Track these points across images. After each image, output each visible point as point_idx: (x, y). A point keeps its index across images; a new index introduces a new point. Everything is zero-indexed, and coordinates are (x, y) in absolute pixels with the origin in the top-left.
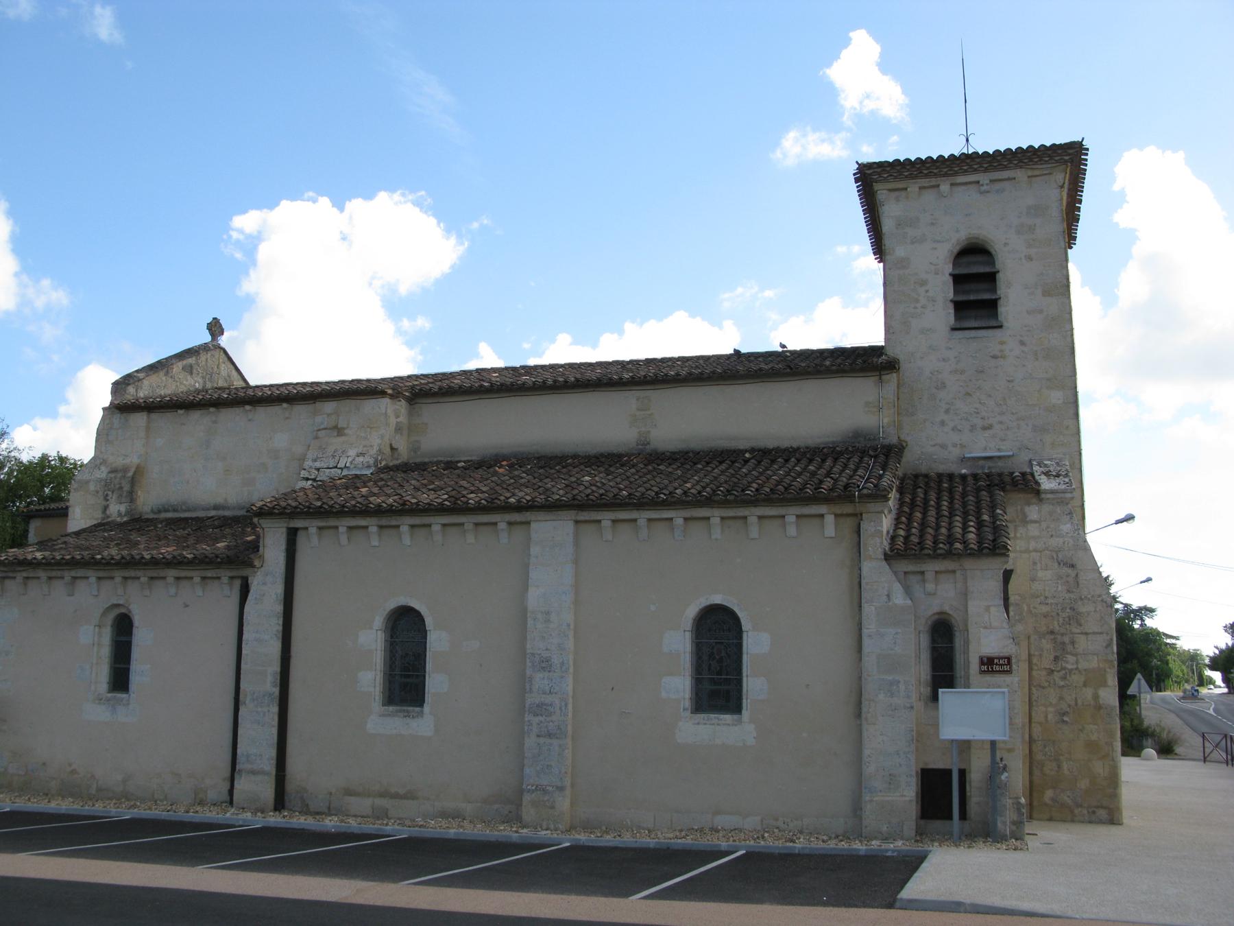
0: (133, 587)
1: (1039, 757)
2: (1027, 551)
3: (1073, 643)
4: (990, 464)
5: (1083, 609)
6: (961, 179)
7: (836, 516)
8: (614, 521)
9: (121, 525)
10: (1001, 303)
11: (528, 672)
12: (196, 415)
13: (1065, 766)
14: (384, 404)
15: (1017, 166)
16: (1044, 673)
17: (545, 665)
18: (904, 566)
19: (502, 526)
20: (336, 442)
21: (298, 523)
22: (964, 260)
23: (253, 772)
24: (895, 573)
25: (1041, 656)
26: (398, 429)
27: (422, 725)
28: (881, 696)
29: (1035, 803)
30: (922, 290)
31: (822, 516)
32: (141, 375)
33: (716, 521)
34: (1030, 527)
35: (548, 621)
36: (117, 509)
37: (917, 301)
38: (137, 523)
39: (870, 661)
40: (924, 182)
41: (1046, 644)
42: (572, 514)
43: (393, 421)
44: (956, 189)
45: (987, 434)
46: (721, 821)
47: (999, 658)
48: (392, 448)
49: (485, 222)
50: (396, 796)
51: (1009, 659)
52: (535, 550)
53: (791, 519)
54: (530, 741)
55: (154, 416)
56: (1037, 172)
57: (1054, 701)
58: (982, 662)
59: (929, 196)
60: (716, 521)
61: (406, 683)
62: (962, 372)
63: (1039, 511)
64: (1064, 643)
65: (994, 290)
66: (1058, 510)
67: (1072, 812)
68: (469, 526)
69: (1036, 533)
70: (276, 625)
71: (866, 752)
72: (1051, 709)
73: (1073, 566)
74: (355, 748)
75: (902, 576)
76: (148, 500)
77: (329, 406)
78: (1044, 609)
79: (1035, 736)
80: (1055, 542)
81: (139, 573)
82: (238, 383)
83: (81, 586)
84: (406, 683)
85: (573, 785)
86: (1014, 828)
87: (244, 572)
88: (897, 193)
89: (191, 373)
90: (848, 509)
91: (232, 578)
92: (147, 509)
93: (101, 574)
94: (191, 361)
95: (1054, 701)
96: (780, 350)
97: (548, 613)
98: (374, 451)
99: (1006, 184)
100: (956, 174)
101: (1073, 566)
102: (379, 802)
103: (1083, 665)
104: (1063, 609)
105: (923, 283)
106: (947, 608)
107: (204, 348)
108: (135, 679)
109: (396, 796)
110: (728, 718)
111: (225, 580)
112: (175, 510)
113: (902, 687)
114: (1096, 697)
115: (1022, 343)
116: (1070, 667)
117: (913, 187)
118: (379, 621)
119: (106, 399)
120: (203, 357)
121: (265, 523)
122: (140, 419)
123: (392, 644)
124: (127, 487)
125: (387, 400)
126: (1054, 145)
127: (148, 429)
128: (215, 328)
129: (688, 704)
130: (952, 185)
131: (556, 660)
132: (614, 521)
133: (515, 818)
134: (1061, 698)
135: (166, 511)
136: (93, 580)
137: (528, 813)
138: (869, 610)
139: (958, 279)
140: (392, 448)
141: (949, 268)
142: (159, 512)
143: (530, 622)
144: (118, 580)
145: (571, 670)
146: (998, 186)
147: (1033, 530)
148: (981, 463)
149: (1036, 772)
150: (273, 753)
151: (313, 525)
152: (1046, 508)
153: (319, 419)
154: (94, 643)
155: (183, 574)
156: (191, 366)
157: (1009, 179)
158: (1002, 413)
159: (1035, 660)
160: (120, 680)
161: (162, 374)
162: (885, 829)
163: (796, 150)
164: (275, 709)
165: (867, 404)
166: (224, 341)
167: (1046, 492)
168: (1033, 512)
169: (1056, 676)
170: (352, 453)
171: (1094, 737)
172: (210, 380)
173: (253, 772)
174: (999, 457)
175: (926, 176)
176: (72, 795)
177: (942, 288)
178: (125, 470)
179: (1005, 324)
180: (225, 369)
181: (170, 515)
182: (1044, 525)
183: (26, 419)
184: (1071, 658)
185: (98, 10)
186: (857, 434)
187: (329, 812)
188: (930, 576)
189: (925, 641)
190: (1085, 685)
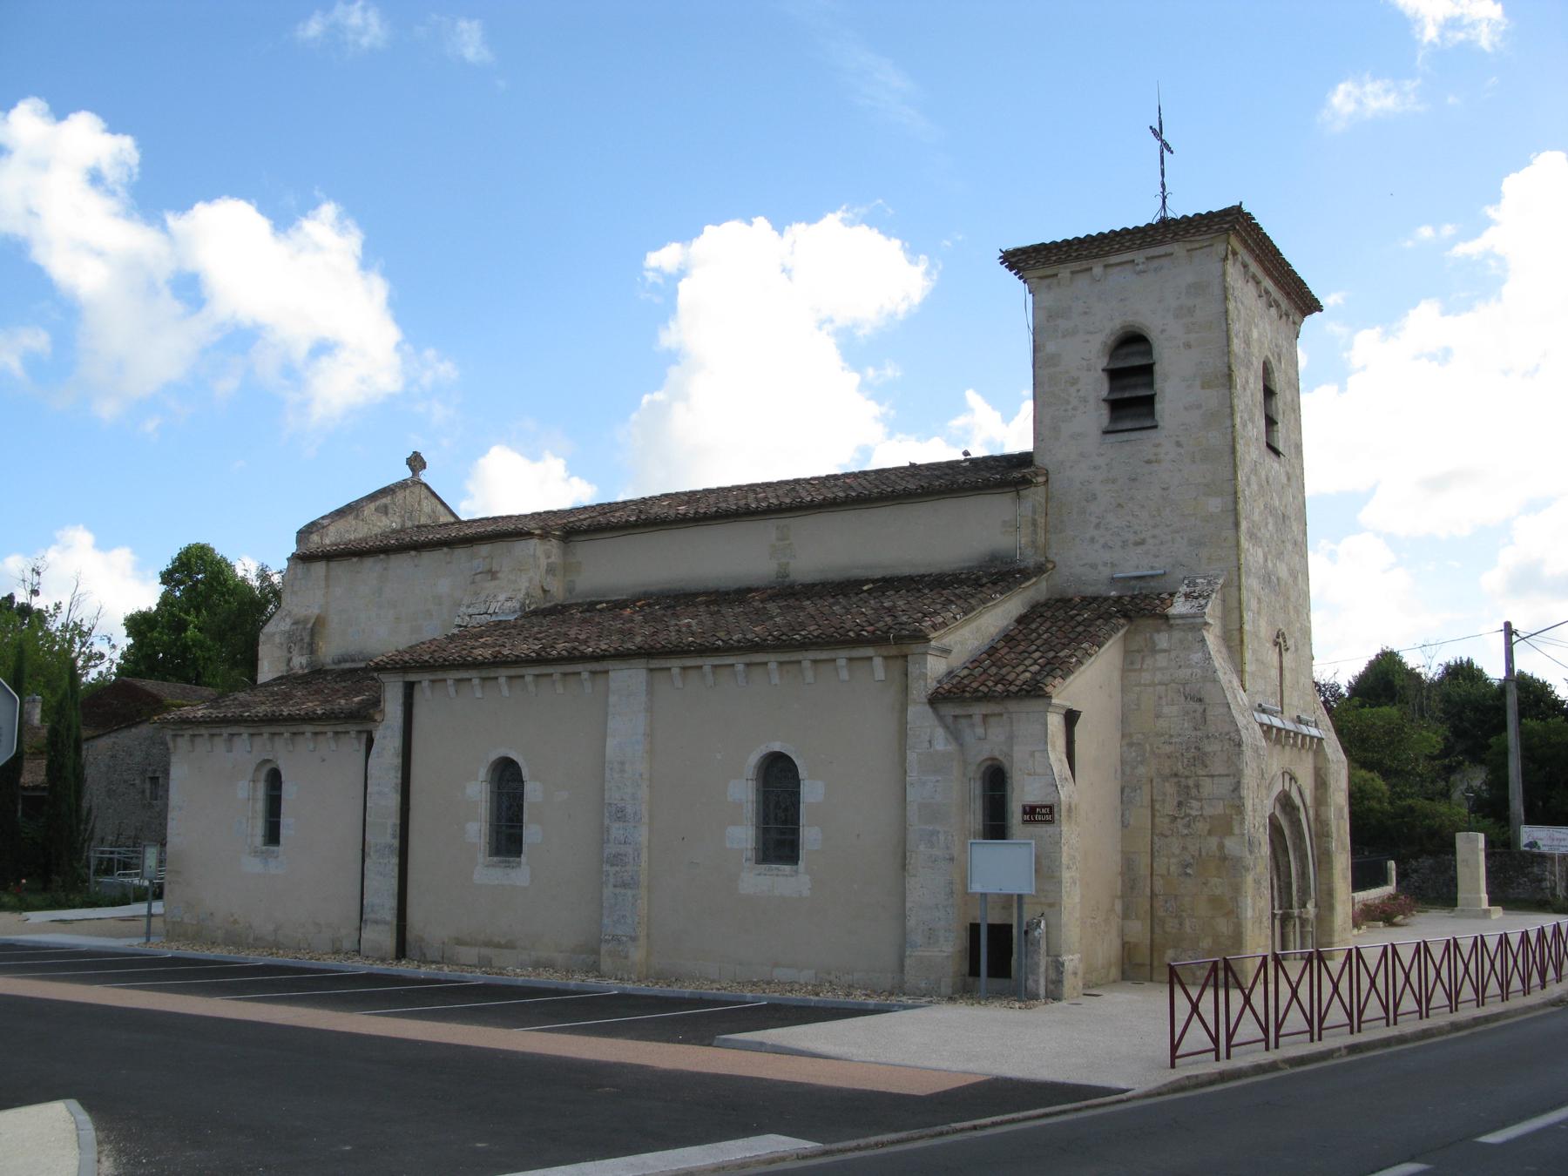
0: (279, 743)
1: (1161, 913)
2: (1153, 684)
3: (1197, 786)
4: (1142, 584)
5: (1208, 749)
6: (1113, 259)
7: (885, 658)
8: (748, 665)
9: (304, 675)
10: (1157, 399)
11: (607, 822)
12: (369, 562)
13: (1187, 923)
14: (533, 546)
15: (1174, 240)
16: (1167, 820)
17: (620, 815)
18: (949, 710)
19: (585, 675)
20: (490, 586)
21: (412, 677)
22: (1124, 351)
23: (376, 922)
24: (941, 718)
25: (1164, 801)
26: (551, 570)
27: (520, 875)
28: (922, 848)
29: (1156, 963)
30: (1072, 390)
31: (870, 658)
32: (325, 522)
33: (773, 666)
34: (1159, 657)
35: (622, 771)
36: (299, 661)
37: (1068, 403)
38: (317, 673)
39: (912, 810)
40: (1075, 266)
41: (1170, 788)
42: (642, 663)
43: (543, 562)
44: (1110, 271)
45: (1139, 550)
46: (780, 974)
47: (1042, 807)
48: (544, 591)
49: (960, 238)
50: (498, 946)
51: (1051, 808)
52: (612, 699)
53: (842, 662)
54: (608, 891)
55: (333, 564)
56: (1197, 245)
57: (1177, 852)
58: (1025, 812)
59: (1082, 281)
60: (773, 666)
61: (507, 837)
62: (1114, 481)
63: (1170, 638)
64: (1188, 787)
65: (1151, 384)
66: (1190, 636)
67: (1194, 974)
68: (557, 677)
69: (1164, 664)
70: (394, 778)
71: (908, 905)
72: (1173, 860)
73: (1200, 700)
74: (476, 904)
75: (950, 720)
76: (330, 650)
77: (484, 549)
78: (1168, 749)
79: (1157, 890)
80: (1184, 673)
81: (282, 729)
82: (445, 518)
83: (237, 742)
84: (507, 837)
85: (648, 936)
86: (1051, 987)
87: (369, 726)
88: (1048, 281)
89: (386, 514)
90: (893, 651)
91: (359, 732)
92: (329, 660)
93: (251, 731)
94: (386, 500)
95: (1177, 852)
96: (962, 458)
97: (622, 763)
98: (521, 596)
99: (1164, 261)
100: (1107, 254)
101: (1200, 700)
102: (485, 951)
103: (1208, 811)
104: (1188, 749)
105: (1074, 381)
106: (997, 754)
107: (403, 485)
108: (284, 832)
109: (498, 946)
110: (787, 868)
111: (353, 734)
112: (353, 661)
113: (942, 838)
114: (1221, 847)
115: (1178, 444)
116: (1194, 813)
117: (1064, 272)
118: (483, 772)
119: (292, 548)
120: (400, 495)
121: (383, 677)
122: (319, 568)
123: (500, 795)
124: (307, 639)
125: (535, 541)
126: (1210, 213)
127: (327, 578)
128: (416, 462)
129: (750, 854)
130: (1106, 266)
131: (629, 810)
132: (748, 665)
133: (594, 969)
134: (1184, 848)
135: (346, 661)
136: (245, 736)
137: (606, 964)
138: (912, 757)
139: (1114, 375)
140: (544, 591)
141: (1103, 362)
142: (340, 662)
143: (607, 771)
144: (266, 736)
145: (646, 819)
146: (1156, 263)
147: (1161, 661)
148: (1133, 583)
149: (1157, 930)
150: (394, 903)
151: (425, 679)
152: (1177, 635)
153: (475, 563)
154: (248, 796)
155: (319, 729)
156: (386, 507)
157: (1166, 255)
158: (1155, 526)
159: (1157, 806)
160: (273, 835)
161: (350, 518)
162: (923, 985)
163: (1350, 107)
164: (395, 860)
165: (1004, 522)
166: (424, 476)
167: (1176, 617)
168: (1162, 640)
169: (1180, 823)
170: (502, 597)
171: (1218, 892)
172: (410, 519)
173: (376, 922)
174: (1152, 576)
175: (1077, 258)
176: (234, 944)
177: (1097, 386)
178: (305, 621)
179: (1161, 424)
180: (428, 505)
181: (347, 666)
182: (1173, 654)
183: (978, 391)
184: (1195, 804)
185: (463, 24)
186: (994, 558)
187: (443, 960)
188: (977, 719)
189: (977, 788)
190: (1210, 833)
